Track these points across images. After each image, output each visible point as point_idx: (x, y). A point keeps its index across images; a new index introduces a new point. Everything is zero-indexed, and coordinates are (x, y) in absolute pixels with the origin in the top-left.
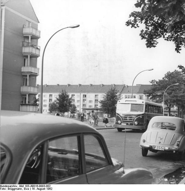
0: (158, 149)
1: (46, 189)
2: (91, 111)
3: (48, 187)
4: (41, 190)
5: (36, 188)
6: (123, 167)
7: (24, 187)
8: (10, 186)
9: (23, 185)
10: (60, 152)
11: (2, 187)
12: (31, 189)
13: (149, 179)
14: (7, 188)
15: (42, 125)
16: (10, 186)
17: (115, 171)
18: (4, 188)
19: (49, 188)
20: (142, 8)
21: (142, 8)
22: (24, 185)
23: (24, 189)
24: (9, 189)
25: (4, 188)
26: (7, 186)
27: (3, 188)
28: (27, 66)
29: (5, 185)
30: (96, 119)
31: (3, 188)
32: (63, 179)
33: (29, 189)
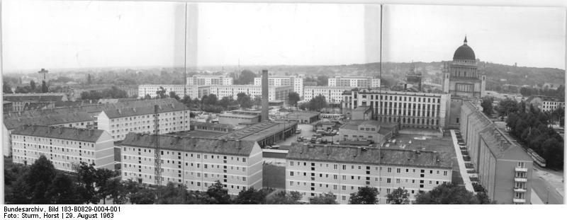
1: (99, 215)
3: (103, 213)
5: (75, 214)
8: (28, 210)
9: (56, 206)
11: (7, 212)
12: (65, 216)
14: (20, 213)
15: (556, 174)
16: (28, 210)
18: (13, 213)
20: (43, 166)
21: (43, 166)
25: (13, 213)
26: (20, 210)
27: (10, 213)
28: (5, 209)
30: (338, 123)
31: (10, 213)
32: (70, 76)
33: (60, 216)
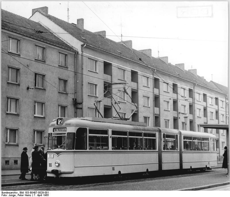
0: (222, 162)
2: (218, 152)
4: (14, 196)
6: (139, 90)
7: (24, 193)
8: (11, 193)
9: (23, 191)
10: (8, 49)
13: (143, 50)
14: (8, 194)
16: (11, 193)
17: (49, 125)
18: (6, 194)
19: (46, 194)
22: (24, 191)
23: (18, 195)
24: (10, 195)
25: (6, 194)
26: (8, 193)
27: (4, 194)
29: (6, 191)
31: (4, 194)
33: (32, 195)
